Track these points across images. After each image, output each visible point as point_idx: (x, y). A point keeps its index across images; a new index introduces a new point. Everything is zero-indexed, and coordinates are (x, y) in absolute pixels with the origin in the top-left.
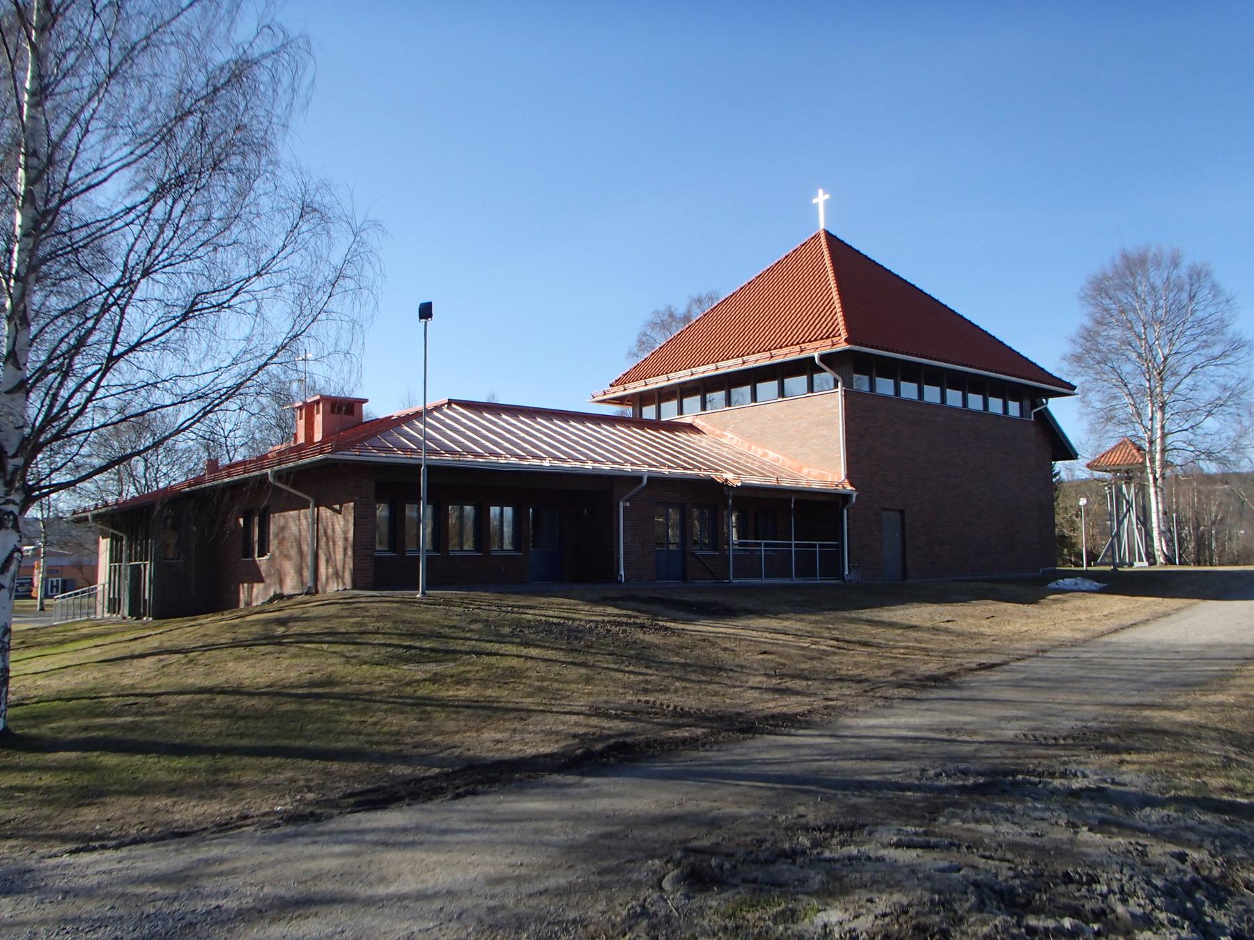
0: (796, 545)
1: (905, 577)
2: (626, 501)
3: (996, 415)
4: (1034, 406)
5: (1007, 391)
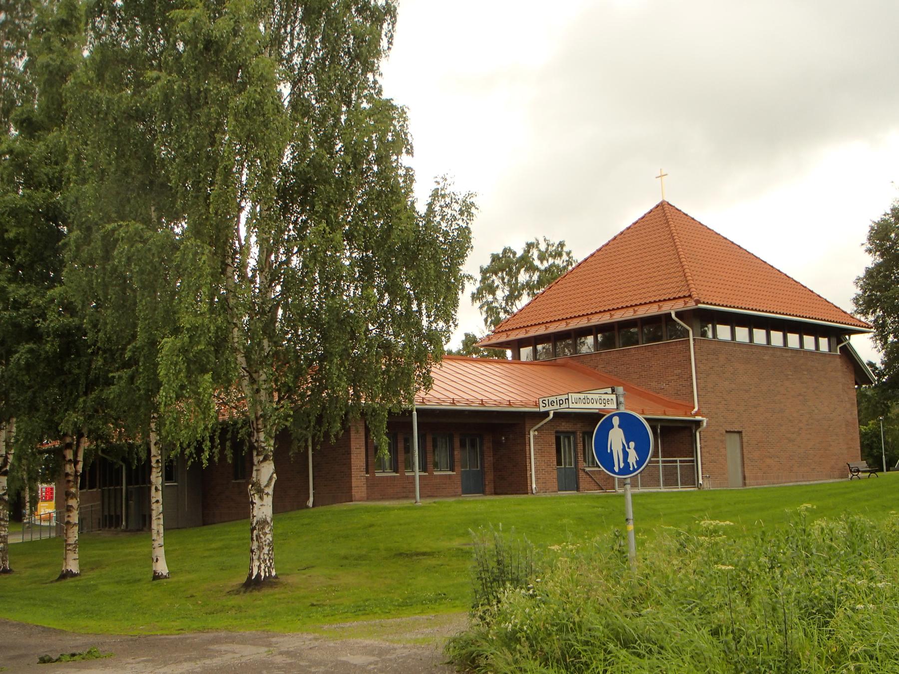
0: (664, 462)
1: (745, 484)
2: (535, 431)
3: (725, 342)
4: (839, 341)
5: (817, 331)
